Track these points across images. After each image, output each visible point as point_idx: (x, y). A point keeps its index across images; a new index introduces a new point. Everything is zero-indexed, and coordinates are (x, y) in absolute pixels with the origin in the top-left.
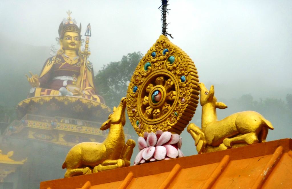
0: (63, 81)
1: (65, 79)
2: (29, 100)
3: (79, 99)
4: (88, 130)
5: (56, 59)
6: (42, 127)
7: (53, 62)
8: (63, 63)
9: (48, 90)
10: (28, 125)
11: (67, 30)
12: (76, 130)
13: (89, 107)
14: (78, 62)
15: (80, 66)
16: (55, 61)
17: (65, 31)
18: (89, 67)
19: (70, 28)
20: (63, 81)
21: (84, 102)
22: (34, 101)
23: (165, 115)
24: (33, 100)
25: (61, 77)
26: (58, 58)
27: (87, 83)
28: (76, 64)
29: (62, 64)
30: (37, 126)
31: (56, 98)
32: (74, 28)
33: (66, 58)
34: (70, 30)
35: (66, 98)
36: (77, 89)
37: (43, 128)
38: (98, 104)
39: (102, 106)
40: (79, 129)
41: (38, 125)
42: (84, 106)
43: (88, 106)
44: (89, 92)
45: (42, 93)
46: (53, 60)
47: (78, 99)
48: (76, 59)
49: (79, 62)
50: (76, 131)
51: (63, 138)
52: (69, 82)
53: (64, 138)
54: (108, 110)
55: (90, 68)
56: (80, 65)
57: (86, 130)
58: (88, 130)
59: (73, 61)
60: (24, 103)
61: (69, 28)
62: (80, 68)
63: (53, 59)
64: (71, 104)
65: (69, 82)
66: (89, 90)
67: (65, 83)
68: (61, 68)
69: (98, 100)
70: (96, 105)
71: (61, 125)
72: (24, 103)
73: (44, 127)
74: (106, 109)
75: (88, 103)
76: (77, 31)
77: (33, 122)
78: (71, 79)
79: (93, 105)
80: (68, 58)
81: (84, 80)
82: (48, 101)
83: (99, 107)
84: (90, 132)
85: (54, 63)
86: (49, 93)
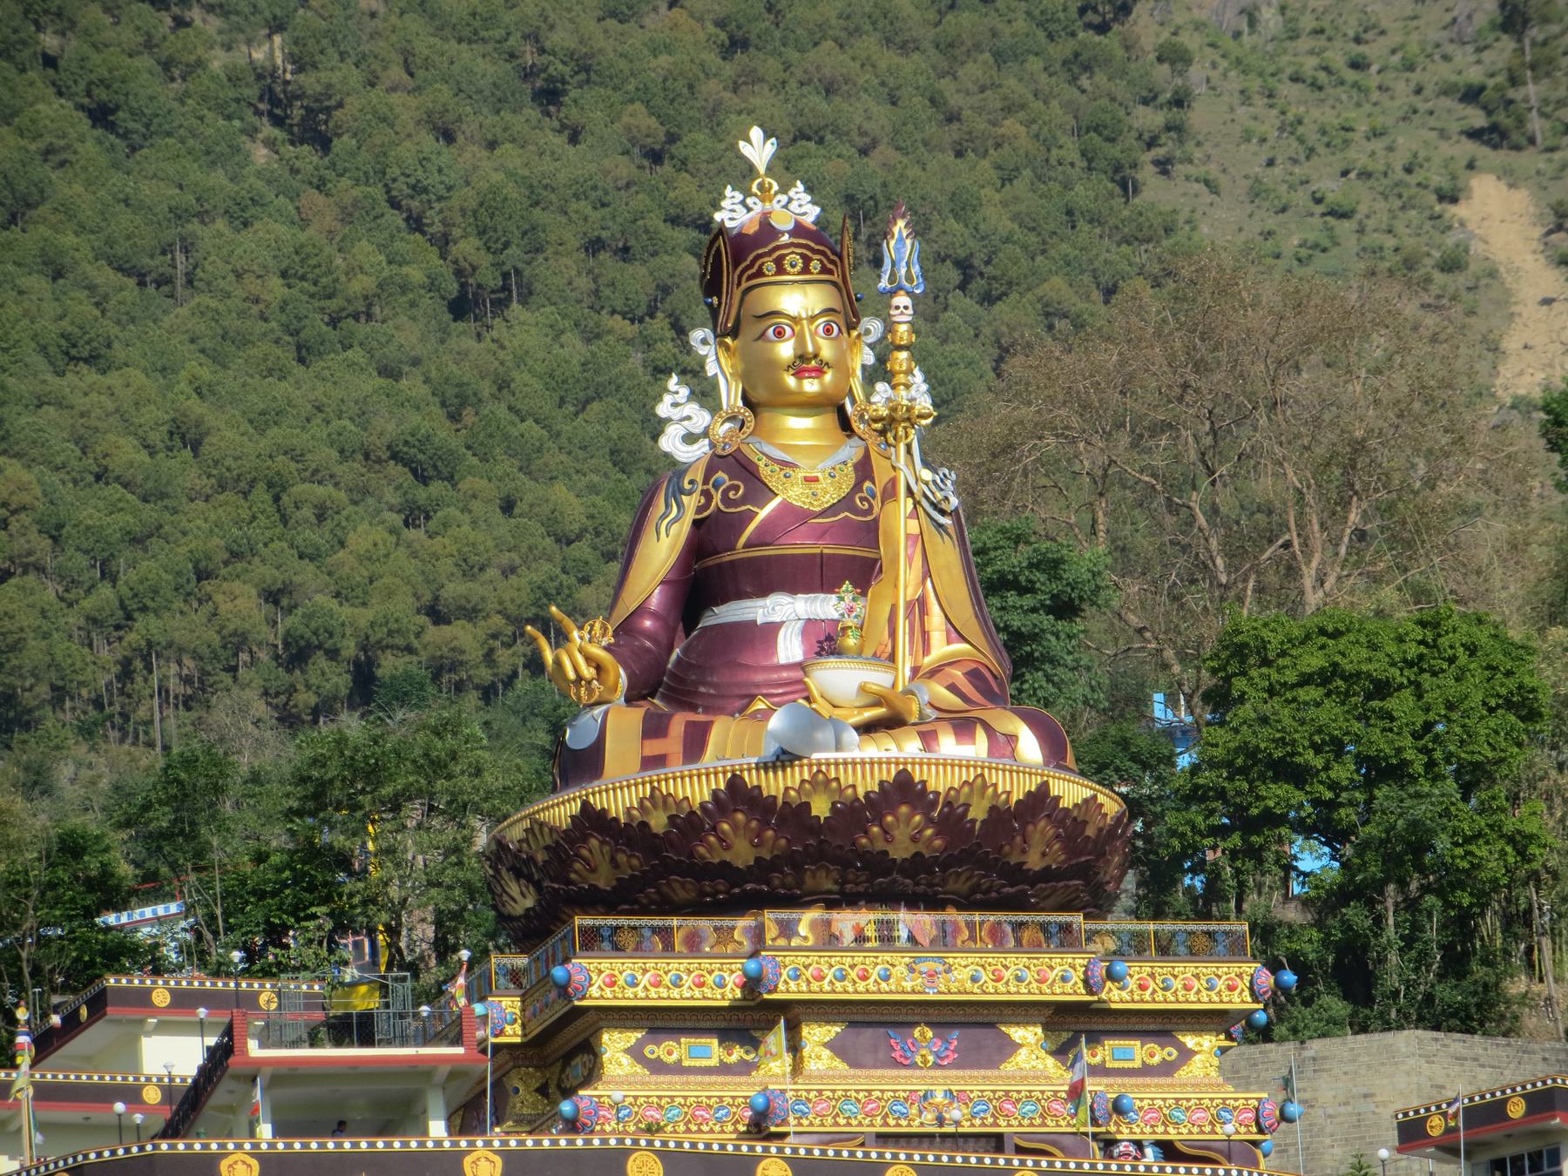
0: (772, 629)
1: (787, 614)
2: (575, 808)
3: (905, 770)
5: (706, 482)
6: (687, 994)
7: (691, 502)
8: (762, 507)
9: (689, 725)
10: (594, 991)
11: (760, 273)
12: (908, 985)
13: (978, 813)
14: (857, 487)
15: (876, 510)
16: (707, 495)
17: (744, 285)
18: (935, 506)
19: (779, 262)
20: (772, 629)
21: (939, 782)
22: (604, 812)
23: (24, 1111)
24: (598, 802)
25: (760, 602)
26: (721, 475)
27: (936, 618)
28: (846, 503)
29: (753, 515)
30: (653, 993)
31: (751, 779)
32: (803, 256)
33: (777, 467)
35: (819, 771)
36: (878, 678)
37: (692, 998)
38: (1032, 784)
39: (1056, 788)
40: (932, 975)
41: (864, 978)
43: (807, 806)
44: (952, 688)
45: (655, 747)
46: (690, 493)
47: (899, 773)
48: (845, 463)
49: (867, 484)
50: (913, 992)
51: (827, 1045)
52: (826, 642)
53: (835, 1047)
54: (1101, 805)
55: (943, 512)
56: (877, 504)
57: (974, 979)
59: (825, 482)
60: (537, 828)
61: (770, 266)
62: (876, 521)
63: (687, 486)
64: (857, 813)
66: (958, 674)
67: (790, 648)
68: (746, 546)
69: (1029, 747)
70: (1017, 788)
71: (852, 967)
72: (542, 825)
73: (697, 994)
74: (1086, 801)
75: (966, 789)
76: (824, 270)
77: (623, 967)
78: (825, 606)
79: (678, 804)
80: (788, 470)
81: (909, 606)
82: (703, 805)
83: (1039, 800)
84: (1001, 986)
85: (699, 510)
86: (695, 744)
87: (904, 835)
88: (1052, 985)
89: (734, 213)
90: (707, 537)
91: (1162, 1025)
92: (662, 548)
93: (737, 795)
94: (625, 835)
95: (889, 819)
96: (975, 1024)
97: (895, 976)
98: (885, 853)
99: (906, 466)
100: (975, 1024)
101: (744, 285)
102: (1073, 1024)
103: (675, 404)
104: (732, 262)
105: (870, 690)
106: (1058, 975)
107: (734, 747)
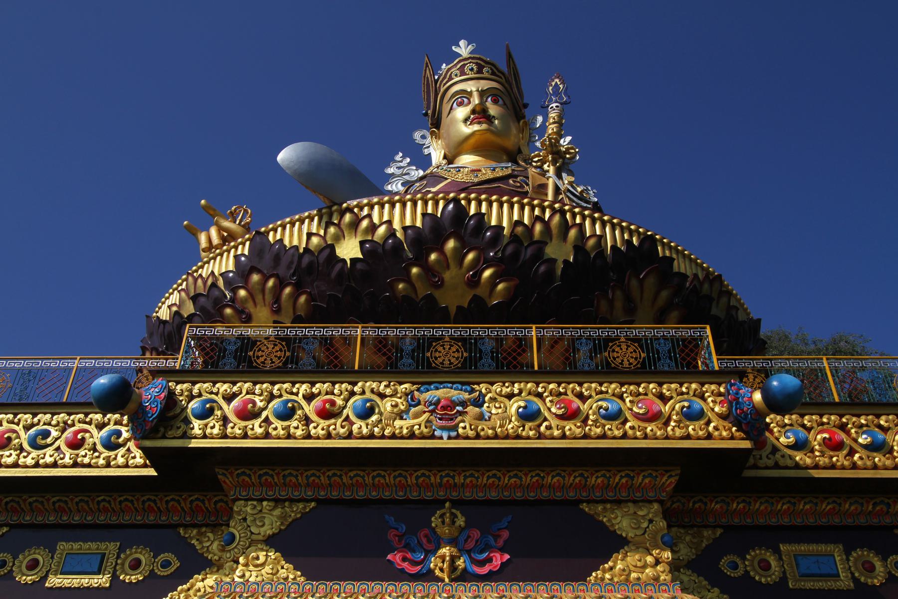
4: (550, 408)
11: (451, 79)
17: (442, 90)
32: (477, 64)
34: (463, 73)
58: (550, 408)
88: (667, 423)
95: (433, 257)
98: (430, 298)
101: (442, 90)
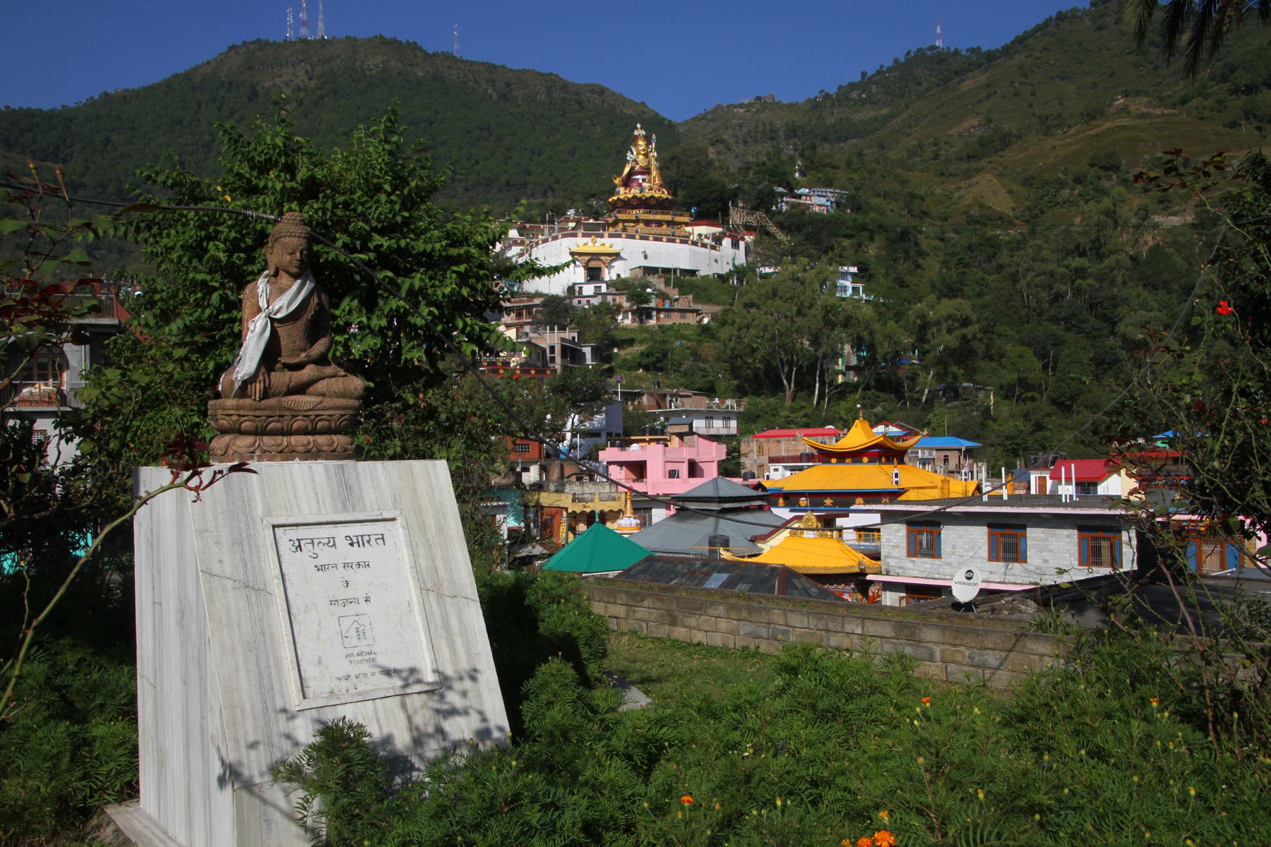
42: (657, 199)
65: (644, 180)
87: (653, 202)
89: (636, 133)
90: (632, 168)
91: (680, 223)
92: (627, 170)
93: (634, 197)
94: (622, 201)
96: (659, 223)
97: (651, 217)
99: (653, 162)
100: (659, 223)
102: (669, 223)
103: (629, 154)
104: (636, 138)
105: (651, 186)
106: (668, 218)
107: (635, 191)
